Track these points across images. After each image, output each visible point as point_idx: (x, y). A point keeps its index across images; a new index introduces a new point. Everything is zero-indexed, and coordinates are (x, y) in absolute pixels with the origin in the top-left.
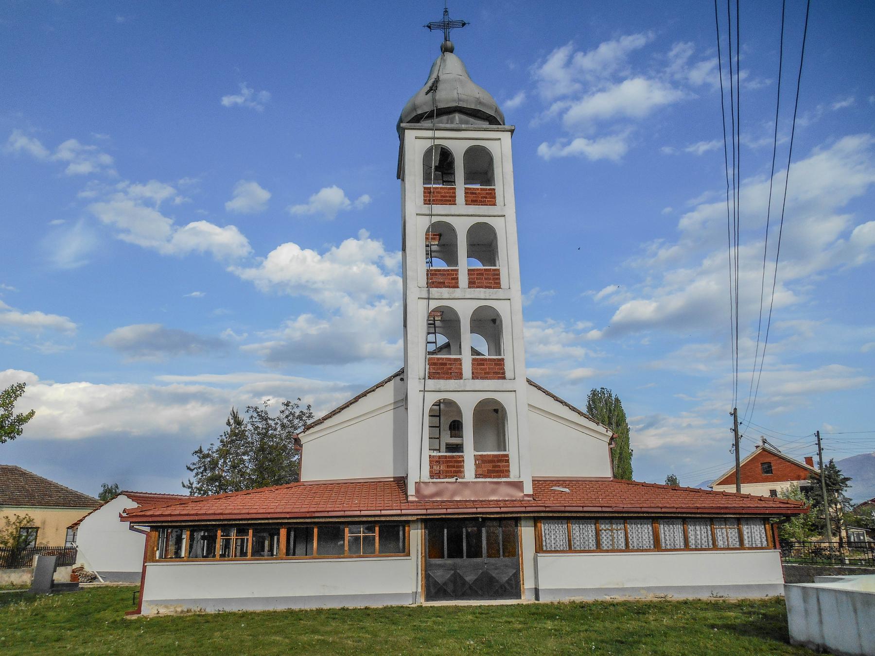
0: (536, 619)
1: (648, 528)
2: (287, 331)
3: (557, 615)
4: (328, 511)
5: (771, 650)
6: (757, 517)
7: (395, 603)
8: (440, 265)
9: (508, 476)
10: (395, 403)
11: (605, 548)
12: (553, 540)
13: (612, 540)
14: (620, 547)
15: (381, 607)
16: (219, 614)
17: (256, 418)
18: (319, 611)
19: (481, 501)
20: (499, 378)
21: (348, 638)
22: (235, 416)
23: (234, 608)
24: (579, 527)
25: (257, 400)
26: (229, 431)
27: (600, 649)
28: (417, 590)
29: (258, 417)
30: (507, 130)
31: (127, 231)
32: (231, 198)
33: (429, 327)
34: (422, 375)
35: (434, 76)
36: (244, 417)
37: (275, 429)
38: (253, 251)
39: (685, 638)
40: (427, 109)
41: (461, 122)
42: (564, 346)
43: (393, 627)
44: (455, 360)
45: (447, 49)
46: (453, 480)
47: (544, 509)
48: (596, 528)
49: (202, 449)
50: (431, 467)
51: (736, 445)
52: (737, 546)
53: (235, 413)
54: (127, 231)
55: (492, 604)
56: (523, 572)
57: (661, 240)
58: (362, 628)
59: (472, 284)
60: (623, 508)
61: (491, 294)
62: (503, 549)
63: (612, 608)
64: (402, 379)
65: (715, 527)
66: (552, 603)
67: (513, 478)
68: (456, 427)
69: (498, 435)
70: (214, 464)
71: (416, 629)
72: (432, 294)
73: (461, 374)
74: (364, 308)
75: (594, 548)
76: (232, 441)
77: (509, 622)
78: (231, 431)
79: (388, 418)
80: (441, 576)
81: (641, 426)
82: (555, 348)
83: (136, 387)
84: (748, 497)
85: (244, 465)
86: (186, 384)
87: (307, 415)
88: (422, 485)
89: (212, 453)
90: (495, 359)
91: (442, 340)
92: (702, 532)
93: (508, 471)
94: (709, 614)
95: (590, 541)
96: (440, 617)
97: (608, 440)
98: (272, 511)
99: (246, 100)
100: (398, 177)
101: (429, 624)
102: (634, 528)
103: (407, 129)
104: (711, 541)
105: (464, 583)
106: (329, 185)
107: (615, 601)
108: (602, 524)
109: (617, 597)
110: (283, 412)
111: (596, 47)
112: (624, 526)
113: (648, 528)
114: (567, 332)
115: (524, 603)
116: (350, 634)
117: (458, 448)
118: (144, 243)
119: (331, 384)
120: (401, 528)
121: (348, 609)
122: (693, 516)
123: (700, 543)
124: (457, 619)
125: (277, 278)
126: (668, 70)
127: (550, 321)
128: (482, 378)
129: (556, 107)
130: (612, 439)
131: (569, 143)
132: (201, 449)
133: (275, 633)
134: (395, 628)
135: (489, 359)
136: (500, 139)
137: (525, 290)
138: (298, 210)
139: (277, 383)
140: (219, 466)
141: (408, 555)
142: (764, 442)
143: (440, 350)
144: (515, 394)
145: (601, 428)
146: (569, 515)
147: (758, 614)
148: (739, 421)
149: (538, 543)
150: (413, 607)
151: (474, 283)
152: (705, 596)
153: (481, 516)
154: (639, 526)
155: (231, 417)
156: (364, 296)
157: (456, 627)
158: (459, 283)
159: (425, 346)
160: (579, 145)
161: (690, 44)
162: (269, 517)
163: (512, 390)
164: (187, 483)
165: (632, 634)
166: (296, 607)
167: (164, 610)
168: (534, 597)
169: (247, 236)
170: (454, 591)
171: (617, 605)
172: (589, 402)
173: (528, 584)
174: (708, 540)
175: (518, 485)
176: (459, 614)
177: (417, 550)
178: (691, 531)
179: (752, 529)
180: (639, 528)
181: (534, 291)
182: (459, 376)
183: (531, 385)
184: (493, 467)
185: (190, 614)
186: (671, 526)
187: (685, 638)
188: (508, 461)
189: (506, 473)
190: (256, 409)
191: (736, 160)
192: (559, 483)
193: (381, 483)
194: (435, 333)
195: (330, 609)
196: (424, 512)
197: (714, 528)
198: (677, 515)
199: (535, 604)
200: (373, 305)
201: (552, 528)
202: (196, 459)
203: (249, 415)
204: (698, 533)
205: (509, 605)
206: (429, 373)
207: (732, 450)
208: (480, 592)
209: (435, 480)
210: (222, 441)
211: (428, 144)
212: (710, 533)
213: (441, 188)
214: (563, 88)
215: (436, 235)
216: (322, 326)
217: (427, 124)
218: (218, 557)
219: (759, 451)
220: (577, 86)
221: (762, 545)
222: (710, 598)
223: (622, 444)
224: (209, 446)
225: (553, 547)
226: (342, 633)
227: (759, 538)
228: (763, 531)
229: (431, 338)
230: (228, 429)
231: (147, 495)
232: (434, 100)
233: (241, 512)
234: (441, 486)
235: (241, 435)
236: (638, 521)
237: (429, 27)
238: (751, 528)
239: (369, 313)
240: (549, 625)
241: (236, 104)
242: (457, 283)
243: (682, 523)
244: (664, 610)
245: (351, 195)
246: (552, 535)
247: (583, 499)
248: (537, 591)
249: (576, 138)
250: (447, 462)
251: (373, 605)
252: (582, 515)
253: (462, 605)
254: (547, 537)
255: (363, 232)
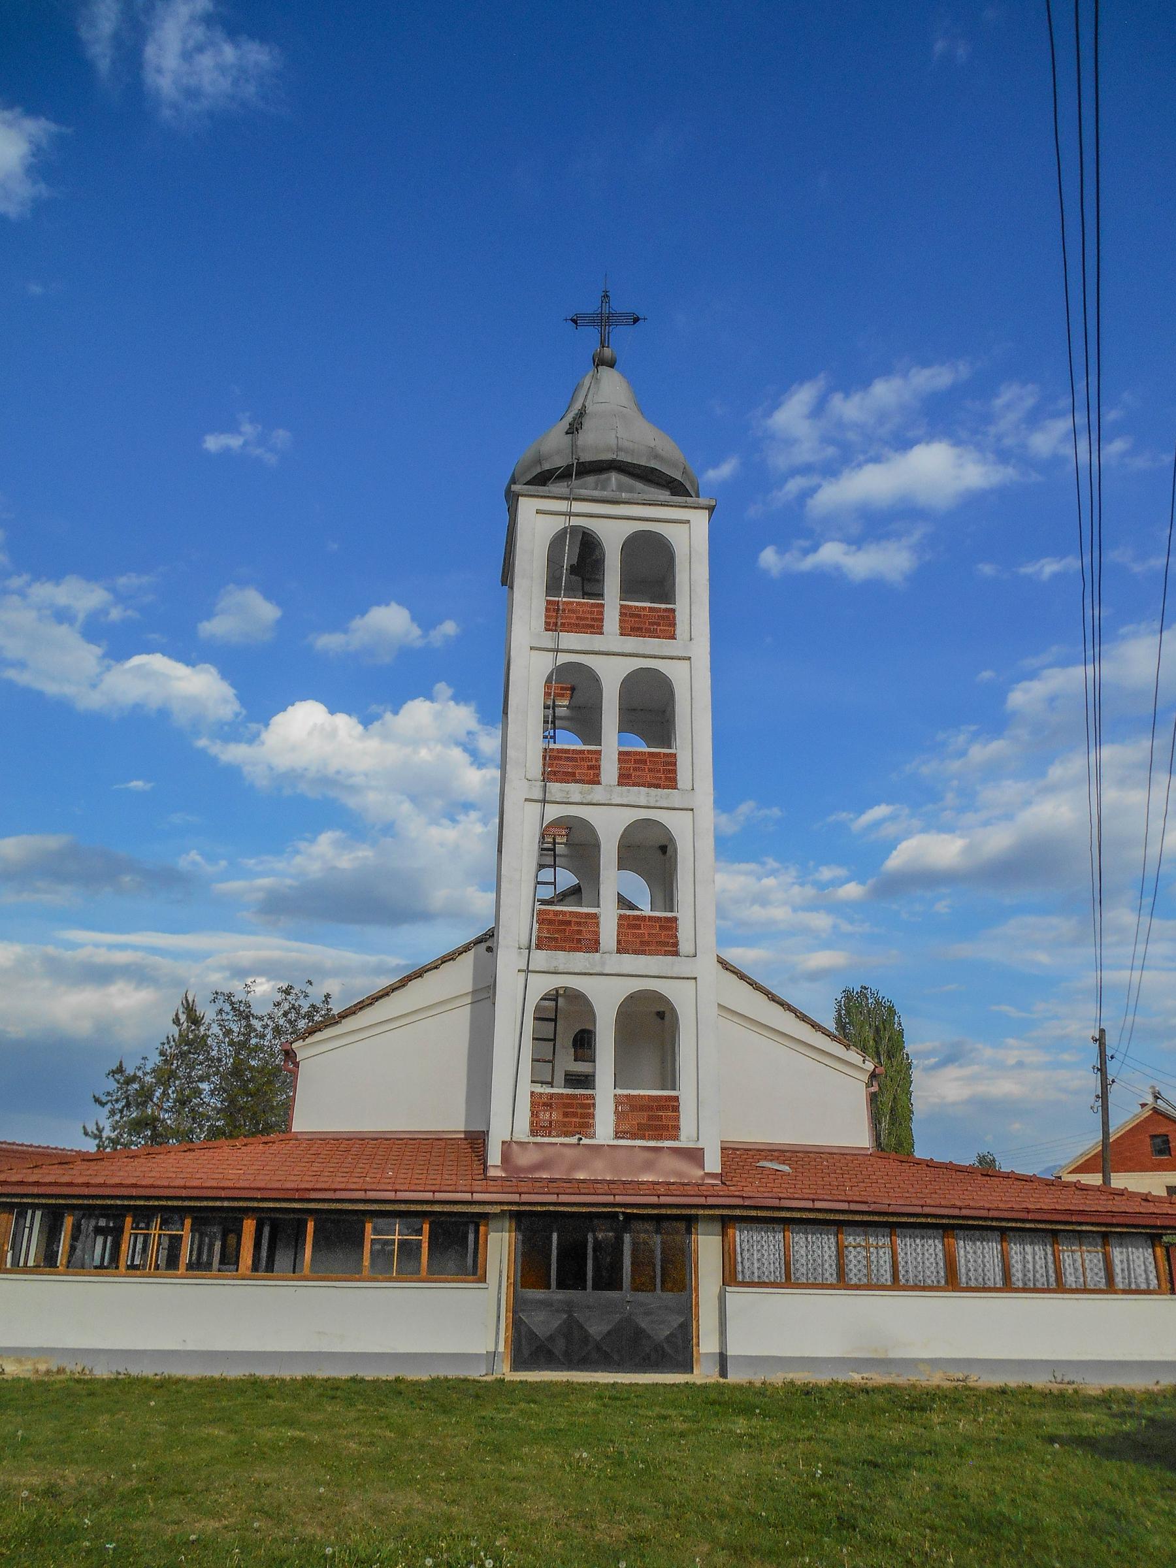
0: (716, 1414)
1: (935, 1246)
2: (298, 859)
3: (758, 1408)
4: (335, 1190)
5: (1163, 1489)
6: (1141, 1233)
7: (452, 1373)
8: (569, 742)
9: (676, 1138)
10: (474, 992)
11: (854, 1281)
12: (755, 1262)
13: (868, 1267)
14: (883, 1280)
15: (425, 1378)
16: (117, 1379)
17: (228, 1014)
18: (308, 1382)
19: (624, 1183)
20: (667, 953)
21: (352, 1436)
22: (190, 1009)
23: (147, 1371)
24: (807, 1238)
25: (237, 983)
26: (177, 1036)
27: (831, 1476)
28: (496, 1349)
29: (232, 1013)
30: (701, 506)
31: (21, 665)
32: (209, 615)
33: (541, 855)
34: (524, 941)
35: (578, 406)
36: (208, 1013)
37: (263, 1036)
38: (244, 712)
39: (997, 1461)
40: (560, 462)
41: (620, 488)
42: (795, 910)
43: (443, 1419)
44: (588, 915)
45: (601, 362)
46: (573, 1140)
47: (739, 1202)
48: (837, 1243)
49: (124, 1066)
50: (534, 1114)
51: (1104, 1097)
52: (1103, 1286)
53: (190, 1001)
54: (21, 665)
55: (636, 1382)
56: (698, 1321)
57: (973, 728)
58: (381, 1419)
59: (625, 779)
60: (889, 1205)
61: (658, 798)
62: (662, 1275)
63: (862, 1397)
64: (489, 949)
65: (1060, 1248)
66: (750, 1383)
67: (684, 1142)
68: (584, 1042)
69: (663, 1061)
70: (146, 1095)
71: (485, 1423)
72: (550, 792)
73: (597, 942)
74: (438, 824)
75: (833, 1280)
76: (183, 1055)
77: (665, 1418)
78: (180, 1036)
79: (460, 1019)
80: (543, 1323)
81: (933, 1060)
82: (780, 914)
83: (18, 949)
84: (1122, 1193)
85: (201, 1099)
86: (112, 947)
87: (323, 1012)
88: (514, 1146)
89: (145, 1074)
90: (659, 918)
91: (566, 879)
92: (1037, 1257)
93: (677, 1128)
94: (1046, 1415)
95: (827, 1266)
96: (535, 1402)
97: (865, 1078)
98: (230, 1184)
99: (246, 444)
100: (504, 583)
101: (511, 1415)
102: (908, 1244)
103: (522, 496)
104: (1054, 1275)
105: (586, 1338)
106: (382, 601)
107: (870, 1384)
108: (849, 1235)
109: (875, 1376)
110: (278, 1004)
111: (865, 384)
112: (891, 1240)
113: (935, 1246)
114: (802, 885)
115: (699, 1382)
116: (356, 1429)
117: (586, 1081)
118: (51, 689)
119: (373, 959)
120: (471, 1228)
121: (362, 1381)
122: (1019, 1225)
123: (1032, 1279)
124: (568, 1407)
125: (283, 762)
126: (992, 430)
127: (772, 863)
128: (636, 952)
129: (794, 486)
130: (873, 1076)
131: (815, 548)
132: (121, 1065)
133: (213, 1422)
134: (446, 1420)
135: (650, 918)
136: (688, 522)
137: (724, 801)
138: (328, 642)
139: (276, 954)
140: (155, 1100)
141: (483, 1279)
142: (1157, 1097)
143: (562, 897)
144: (694, 984)
145: (854, 1056)
146: (788, 1215)
147: (1140, 1417)
148: (1109, 1053)
149: (727, 1267)
150: (486, 1382)
151: (629, 776)
152: (1040, 1382)
153: (623, 1210)
154: (918, 1241)
155: (181, 1010)
156: (438, 804)
157: (562, 1423)
158: (602, 775)
159: (532, 888)
160: (831, 553)
161: (1030, 387)
162: (223, 1196)
163: (689, 976)
164: (91, 1128)
165: (897, 1450)
166: (264, 1372)
167: (14, 1368)
168: (717, 1369)
169: (233, 685)
170: (567, 1354)
171: (873, 1391)
172: (839, 1011)
173: (707, 1344)
174: (1047, 1272)
175: (695, 1156)
176: (572, 1397)
177: (501, 1272)
178: (1016, 1253)
179: (1130, 1254)
180: (918, 1245)
181: (746, 808)
182: (594, 946)
183: (727, 969)
184: (650, 1118)
185: (61, 1377)
186: (978, 1243)
187: (997, 1461)
188: (676, 1109)
189: (673, 1131)
190: (230, 995)
191: (1098, 738)
192: (772, 1155)
193: (440, 1142)
194: (554, 866)
195: (329, 1379)
196: (515, 1198)
197: (1059, 1250)
198: (989, 1223)
199: (718, 1385)
200: (454, 820)
201: (755, 1238)
202: (112, 1085)
203: (217, 1007)
204: (1029, 1258)
205: (670, 1385)
206: (539, 938)
207: (1096, 1107)
208: (616, 1357)
209: (539, 1139)
210: (162, 1054)
211: (559, 523)
212: (1050, 1258)
213: (578, 603)
214: (805, 453)
215: (566, 689)
216: (360, 854)
217: (560, 488)
218: (122, 1269)
219: (1147, 1113)
220: (831, 451)
221: (1148, 1287)
222: (1050, 1385)
223: (896, 1091)
224: (139, 1062)
225: (756, 1274)
226: (340, 1426)
227: (1143, 1273)
228: (1151, 1259)
229: (547, 875)
230: (175, 1031)
231: (15, 1147)
232: (574, 446)
233: (187, 1184)
234: (551, 1151)
235: (200, 1043)
236: (917, 1232)
237: (575, 321)
238: (1128, 1253)
239: (447, 834)
240: (740, 1425)
241: (227, 450)
242: (598, 775)
243: (999, 1239)
244: (960, 1405)
245: (426, 621)
246: (755, 1253)
247: (815, 1187)
248: (723, 1359)
249: (827, 541)
250: (566, 1105)
251: (413, 1376)
252: (812, 1216)
253: (581, 1380)
254: (746, 1255)
255: (442, 689)
